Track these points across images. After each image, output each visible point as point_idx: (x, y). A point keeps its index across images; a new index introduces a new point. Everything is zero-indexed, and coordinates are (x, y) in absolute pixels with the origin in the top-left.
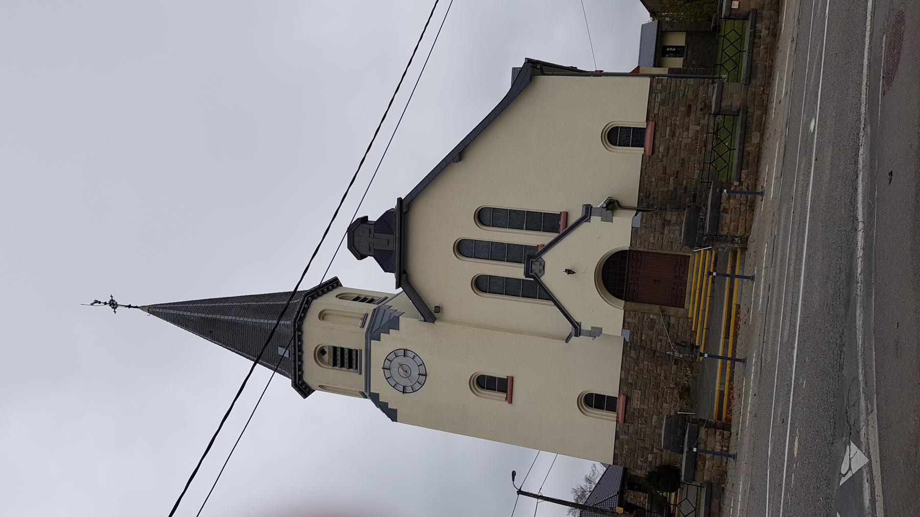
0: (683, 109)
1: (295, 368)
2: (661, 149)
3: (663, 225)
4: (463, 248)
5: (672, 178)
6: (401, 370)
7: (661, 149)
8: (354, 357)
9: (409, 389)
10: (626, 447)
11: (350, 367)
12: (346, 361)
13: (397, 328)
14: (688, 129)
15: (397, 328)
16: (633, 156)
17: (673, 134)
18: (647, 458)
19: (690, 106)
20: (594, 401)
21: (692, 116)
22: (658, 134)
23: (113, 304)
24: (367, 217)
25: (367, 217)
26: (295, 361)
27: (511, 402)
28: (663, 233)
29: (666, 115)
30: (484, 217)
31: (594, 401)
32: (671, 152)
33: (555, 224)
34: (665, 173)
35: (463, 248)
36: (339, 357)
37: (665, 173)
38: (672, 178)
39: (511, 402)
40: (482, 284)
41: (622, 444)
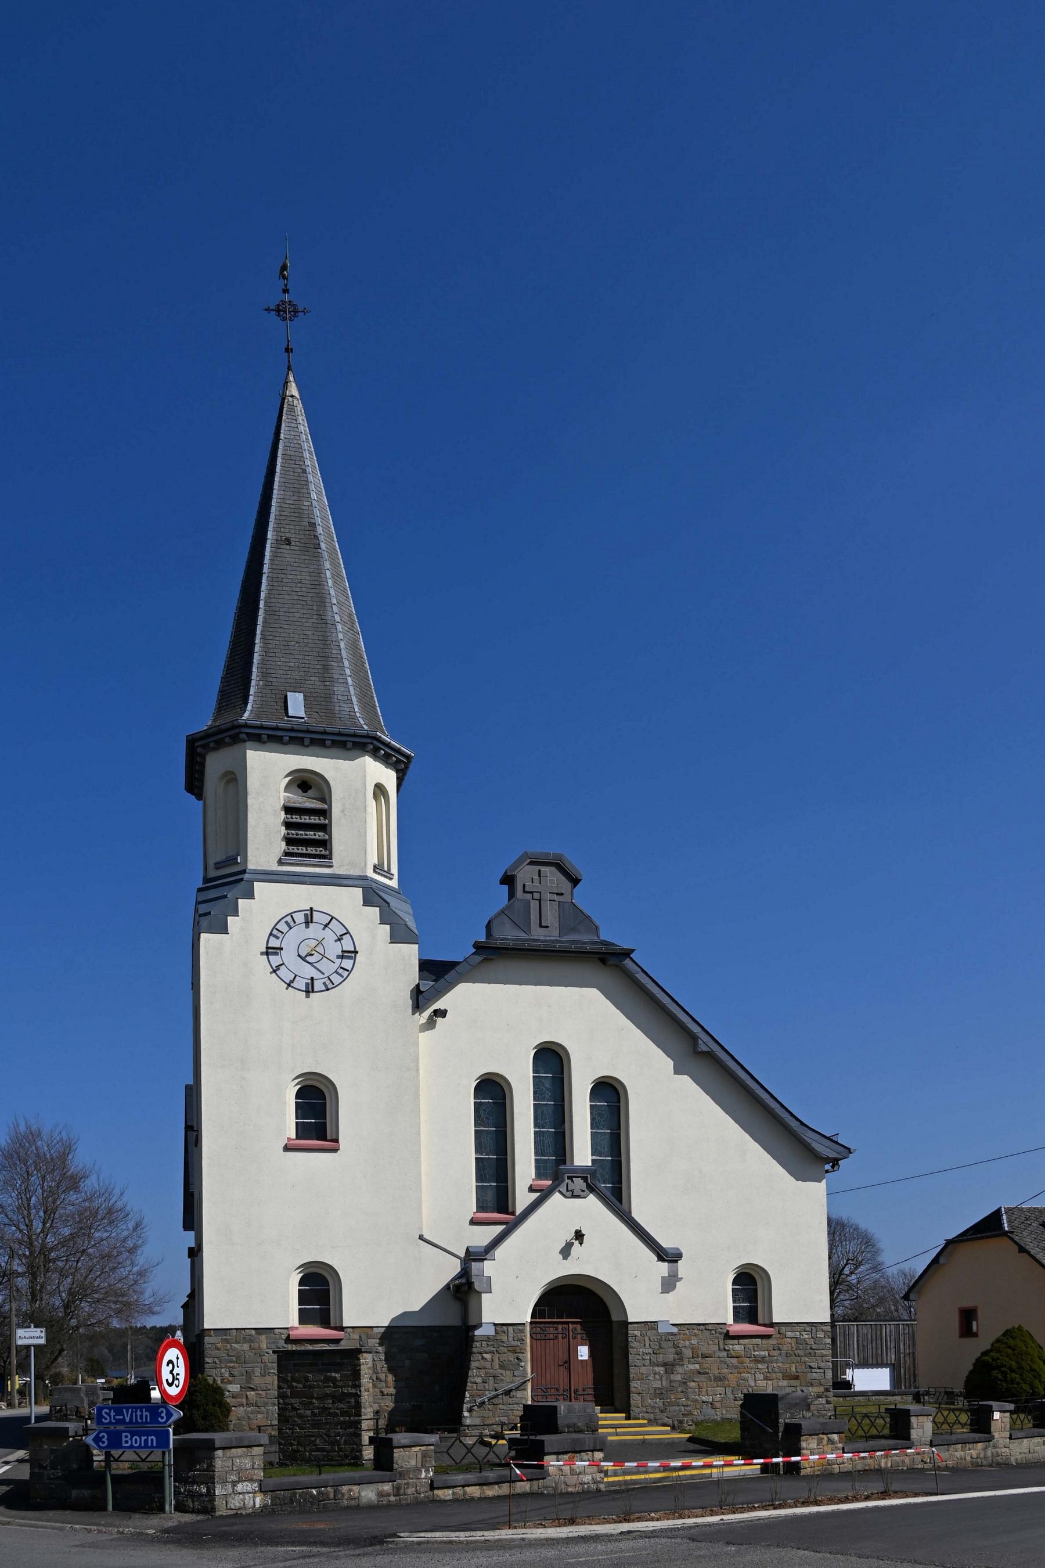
0: (793, 1369)
1: (277, 729)
2: (737, 1348)
3: (665, 1365)
4: (551, 1060)
5: (697, 1366)
6: (313, 943)
7: (737, 1348)
8: (311, 850)
9: (275, 960)
11: (289, 841)
12: (302, 834)
13: (394, 939)
14: (766, 1379)
15: (394, 939)
16: (719, 1307)
17: (758, 1360)
18: (230, 1382)
19: (797, 1378)
20: (318, 1288)
21: (785, 1383)
22: (758, 1341)
23: (287, 350)
24: (190, 1249)
25: (190, 1249)
26: (292, 730)
27: (287, 1149)
28: (652, 1364)
29: (785, 1348)
30: (609, 1094)
31: (318, 1288)
32: (735, 1361)
33: (610, 1181)
34: (704, 1356)
35: (551, 1060)
36: (306, 819)
37: (704, 1356)
38: (697, 1366)
39: (287, 1149)
40: (492, 1092)
41: (251, 1341)
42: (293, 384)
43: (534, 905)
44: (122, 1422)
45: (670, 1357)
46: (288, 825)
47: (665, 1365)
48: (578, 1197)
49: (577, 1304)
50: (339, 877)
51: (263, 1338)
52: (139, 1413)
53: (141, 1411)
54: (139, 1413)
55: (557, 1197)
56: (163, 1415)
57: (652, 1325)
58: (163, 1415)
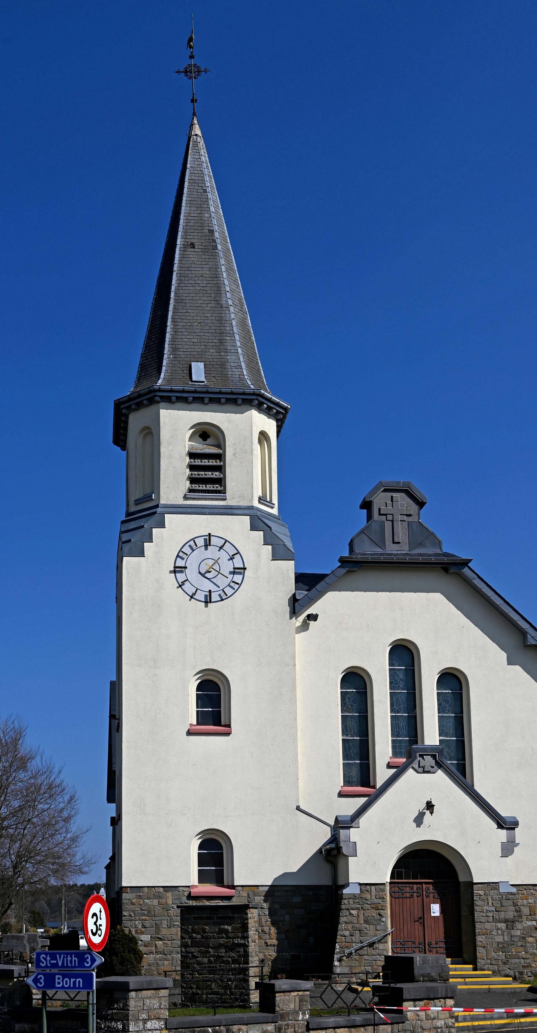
3: (506, 921)
4: (404, 655)
10: (155, 902)
20: (214, 852)
28: (495, 920)
30: (453, 683)
31: (214, 852)
35: (404, 655)
40: (355, 683)
42: (197, 126)
43: (388, 525)
44: (55, 966)
45: (511, 914)
46: (192, 468)
47: (506, 921)
48: (428, 772)
49: (429, 867)
50: (231, 508)
51: (169, 894)
52: (69, 958)
53: (71, 957)
54: (69, 958)
55: (410, 771)
56: (88, 960)
57: (494, 886)
58: (88, 960)
